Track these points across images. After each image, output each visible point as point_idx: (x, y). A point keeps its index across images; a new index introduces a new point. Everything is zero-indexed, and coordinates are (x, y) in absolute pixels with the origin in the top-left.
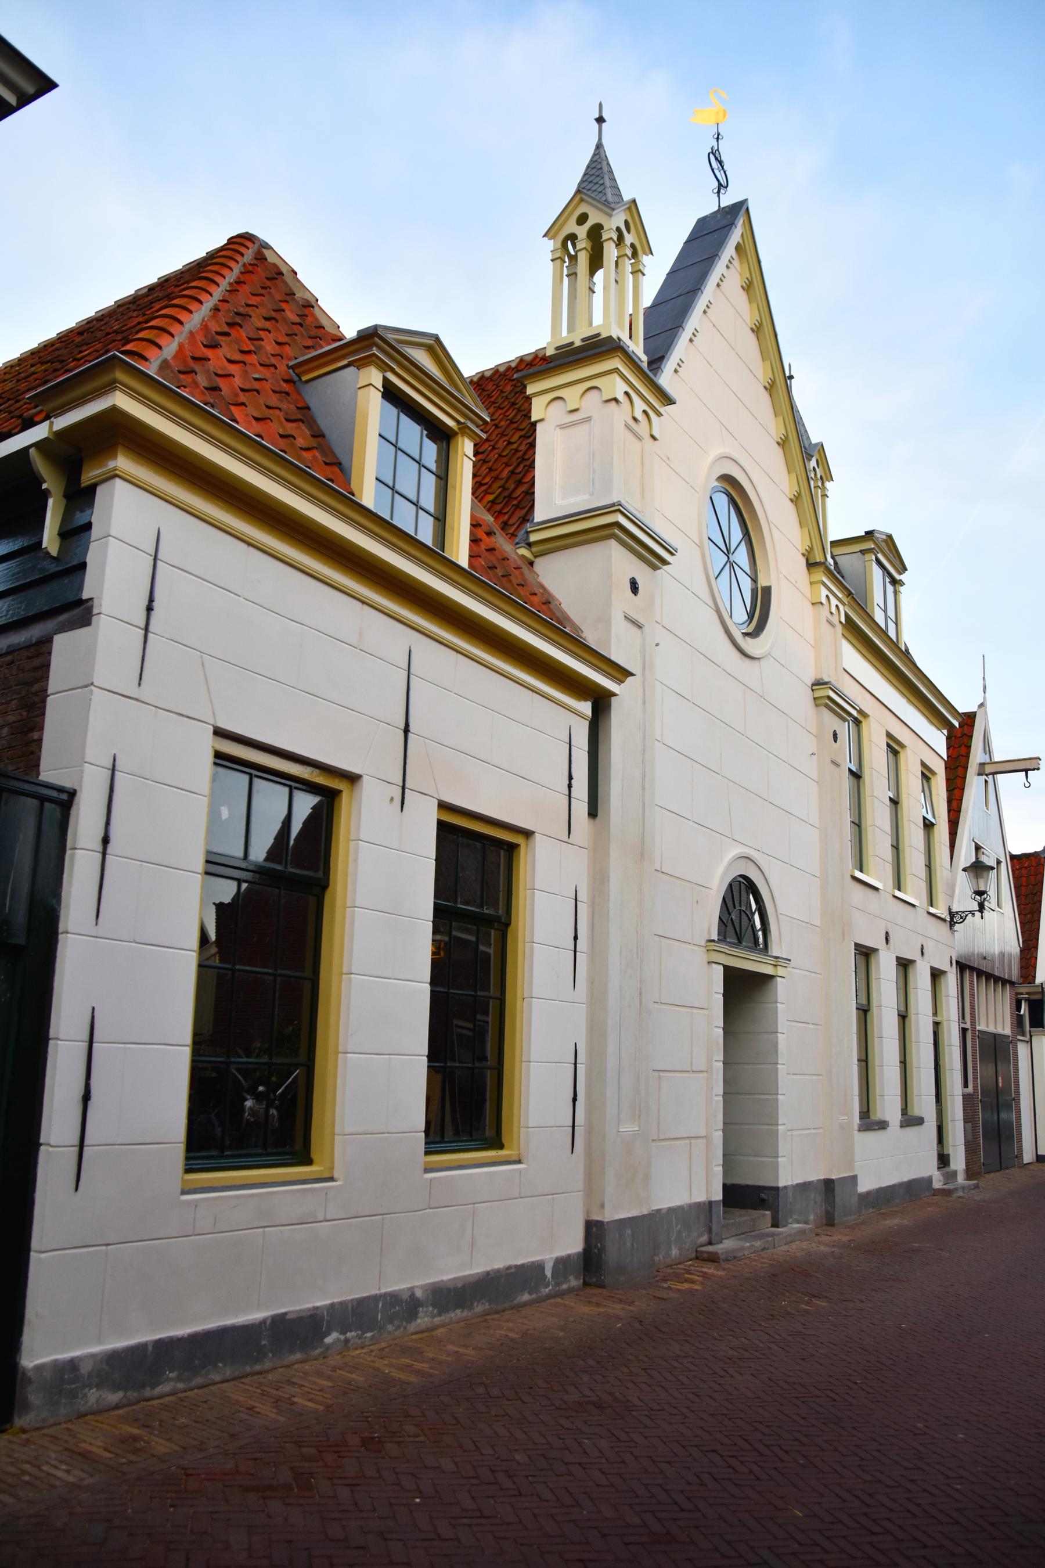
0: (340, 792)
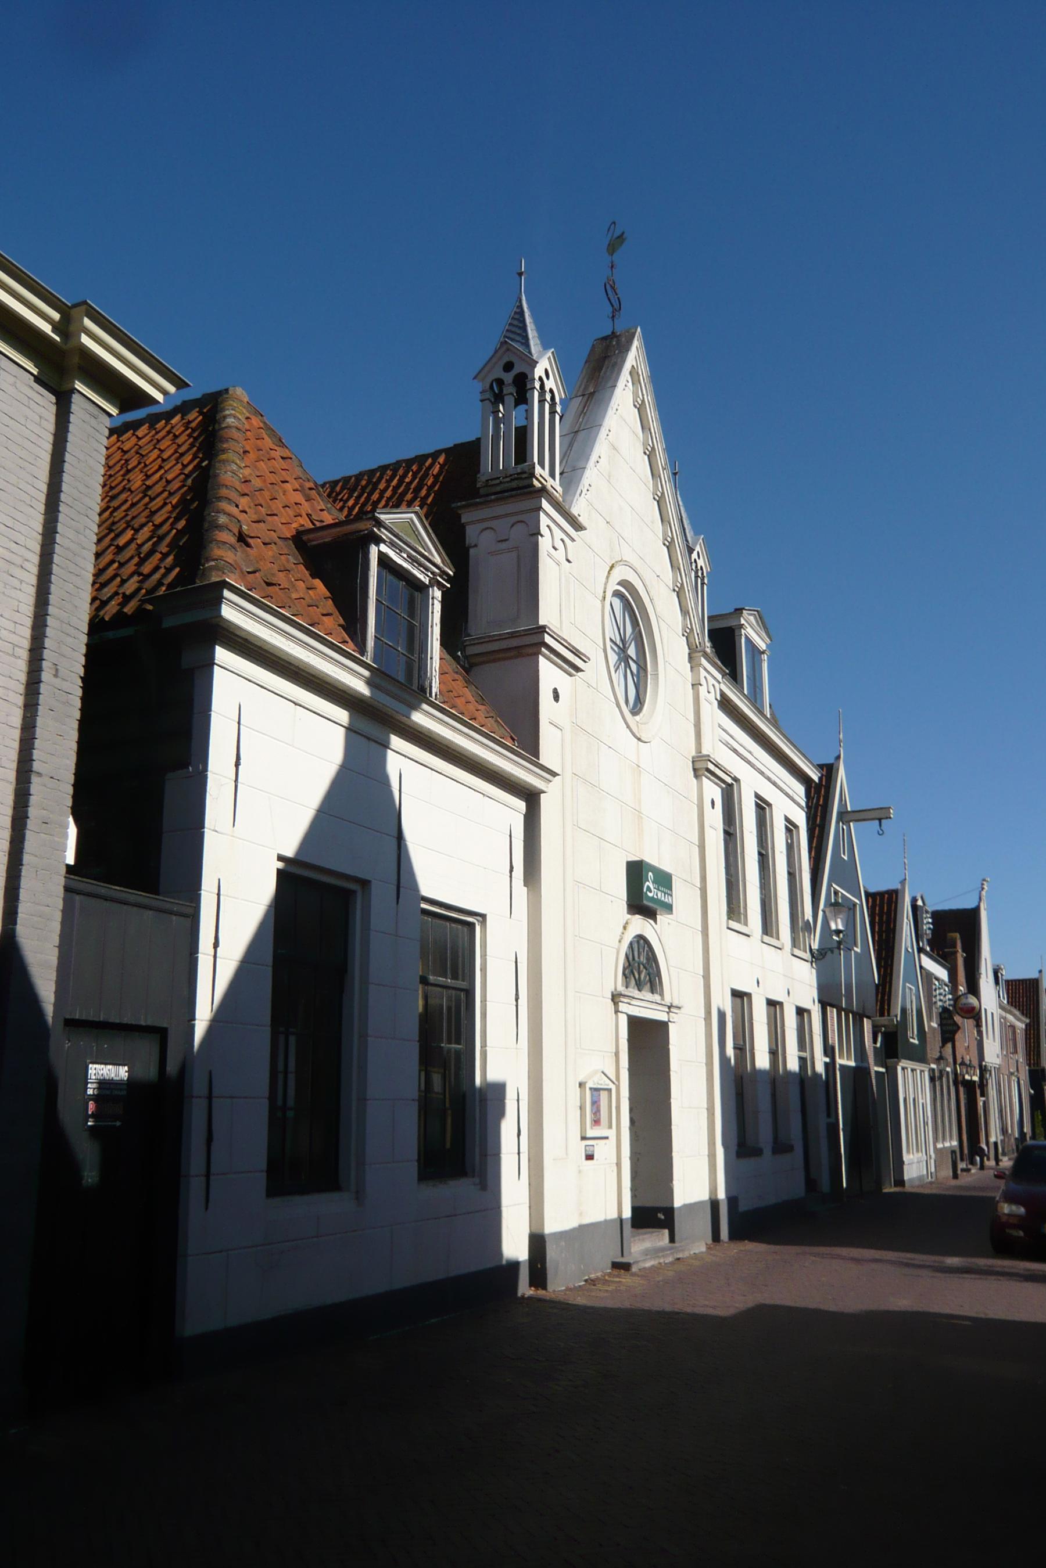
0: (354, 892)
